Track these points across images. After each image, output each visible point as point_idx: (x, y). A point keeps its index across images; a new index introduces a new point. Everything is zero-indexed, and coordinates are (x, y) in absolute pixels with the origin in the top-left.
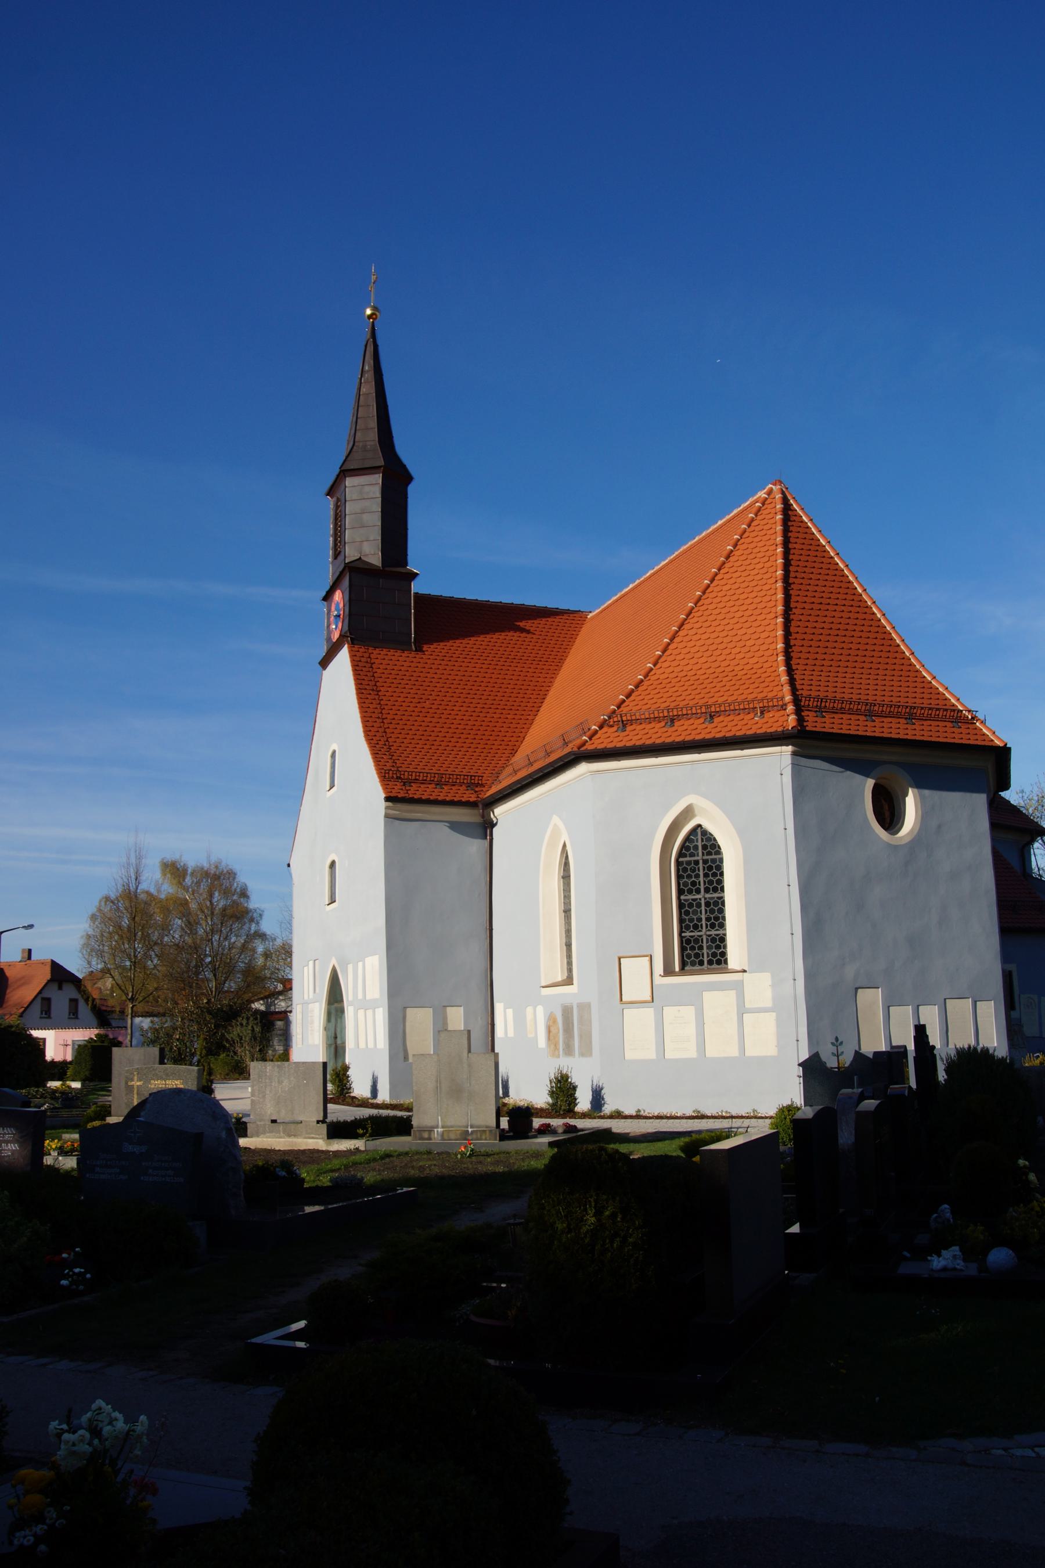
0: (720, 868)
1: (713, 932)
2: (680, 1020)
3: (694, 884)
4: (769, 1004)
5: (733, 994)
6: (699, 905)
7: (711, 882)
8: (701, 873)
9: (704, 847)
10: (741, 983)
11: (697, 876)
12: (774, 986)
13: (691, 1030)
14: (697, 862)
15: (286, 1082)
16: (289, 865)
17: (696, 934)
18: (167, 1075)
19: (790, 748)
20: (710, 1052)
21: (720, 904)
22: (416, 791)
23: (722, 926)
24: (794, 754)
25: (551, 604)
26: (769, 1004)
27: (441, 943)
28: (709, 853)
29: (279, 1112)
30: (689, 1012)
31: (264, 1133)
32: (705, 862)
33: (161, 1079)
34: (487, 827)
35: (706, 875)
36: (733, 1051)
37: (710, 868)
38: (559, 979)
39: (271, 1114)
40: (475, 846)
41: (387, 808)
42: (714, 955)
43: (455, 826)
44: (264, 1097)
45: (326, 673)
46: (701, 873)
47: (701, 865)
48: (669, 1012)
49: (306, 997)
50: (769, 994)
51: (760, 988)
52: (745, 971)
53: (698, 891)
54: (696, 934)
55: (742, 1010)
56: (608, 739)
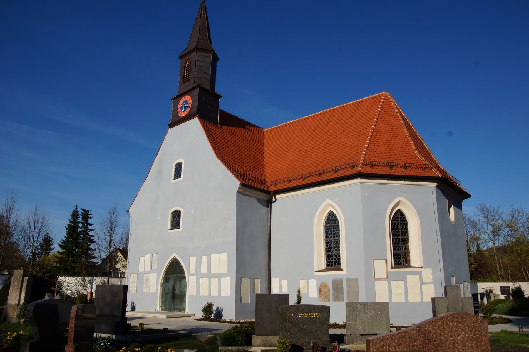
0: (338, 228)
1: (330, 253)
2: (398, 286)
3: (397, 232)
4: (432, 281)
5: (418, 276)
6: (399, 241)
7: (335, 233)
8: (400, 228)
9: (401, 218)
10: (421, 272)
11: (398, 229)
12: (433, 274)
13: (402, 291)
14: (398, 224)
15: (369, 314)
16: (128, 211)
17: (398, 252)
18: (310, 310)
19: (436, 184)
20: (410, 300)
21: (338, 242)
22: (251, 184)
23: (339, 250)
24: (437, 186)
25: (256, 124)
26: (432, 281)
27: (253, 250)
28: (403, 221)
29: (365, 329)
30: (401, 283)
31: (357, 341)
32: (401, 224)
33: (306, 312)
34: (268, 203)
35: (402, 229)
36: (419, 300)
37: (403, 226)
38: (323, 268)
39: (360, 331)
40: (264, 210)
41: (239, 188)
42: (336, 262)
43: (259, 200)
44: (356, 321)
45: (170, 131)
46: (400, 228)
47: (400, 225)
48: (394, 283)
49: (140, 270)
50: (431, 277)
51: (428, 274)
52: (422, 267)
53: (399, 235)
54: (398, 252)
55: (422, 283)
56: (368, 170)
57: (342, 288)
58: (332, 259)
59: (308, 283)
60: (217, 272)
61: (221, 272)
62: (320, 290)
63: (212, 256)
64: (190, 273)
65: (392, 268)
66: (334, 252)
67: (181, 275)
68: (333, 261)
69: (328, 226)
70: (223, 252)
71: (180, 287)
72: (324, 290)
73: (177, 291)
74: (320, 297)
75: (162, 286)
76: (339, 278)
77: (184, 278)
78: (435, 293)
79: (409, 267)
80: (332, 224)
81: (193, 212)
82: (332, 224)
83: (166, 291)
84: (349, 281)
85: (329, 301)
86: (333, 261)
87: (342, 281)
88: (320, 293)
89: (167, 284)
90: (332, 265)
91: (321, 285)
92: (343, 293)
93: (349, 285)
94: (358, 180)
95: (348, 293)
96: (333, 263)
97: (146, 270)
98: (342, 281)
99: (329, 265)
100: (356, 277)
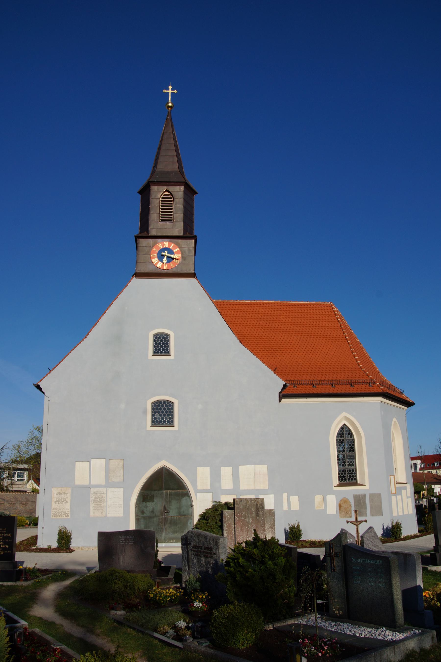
10: (406, 487)
57: (365, 503)
58: (345, 474)
59: (325, 500)
60: (252, 488)
61: (258, 487)
62: (340, 506)
63: (242, 469)
64: (199, 487)
65: (340, 485)
66: (348, 467)
67: (180, 491)
68: (348, 476)
69: (340, 440)
70: (261, 463)
71: (180, 508)
72: (344, 506)
73: (173, 513)
74: (340, 513)
75: (136, 507)
76: (360, 493)
77: (187, 494)
78: (136, 528)
79: (356, 484)
80: (345, 438)
81: (200, 406)
82: (345, 438)
83: (147, 514)
84: (371, 496)
85: (366, 516)
86: (348, 476)
87: (364, 496)
88: (340, 509)
89: (150, 505)
90: (345, 480)
91: (341, 501)
92: (366, 508)
93: (371, 500)
94: (380, 399)
95: (371, 508)
96: (347, 478)
97: (93, 483)
98: (364, 496)
99: (342, 480)
100: (378, 492)
